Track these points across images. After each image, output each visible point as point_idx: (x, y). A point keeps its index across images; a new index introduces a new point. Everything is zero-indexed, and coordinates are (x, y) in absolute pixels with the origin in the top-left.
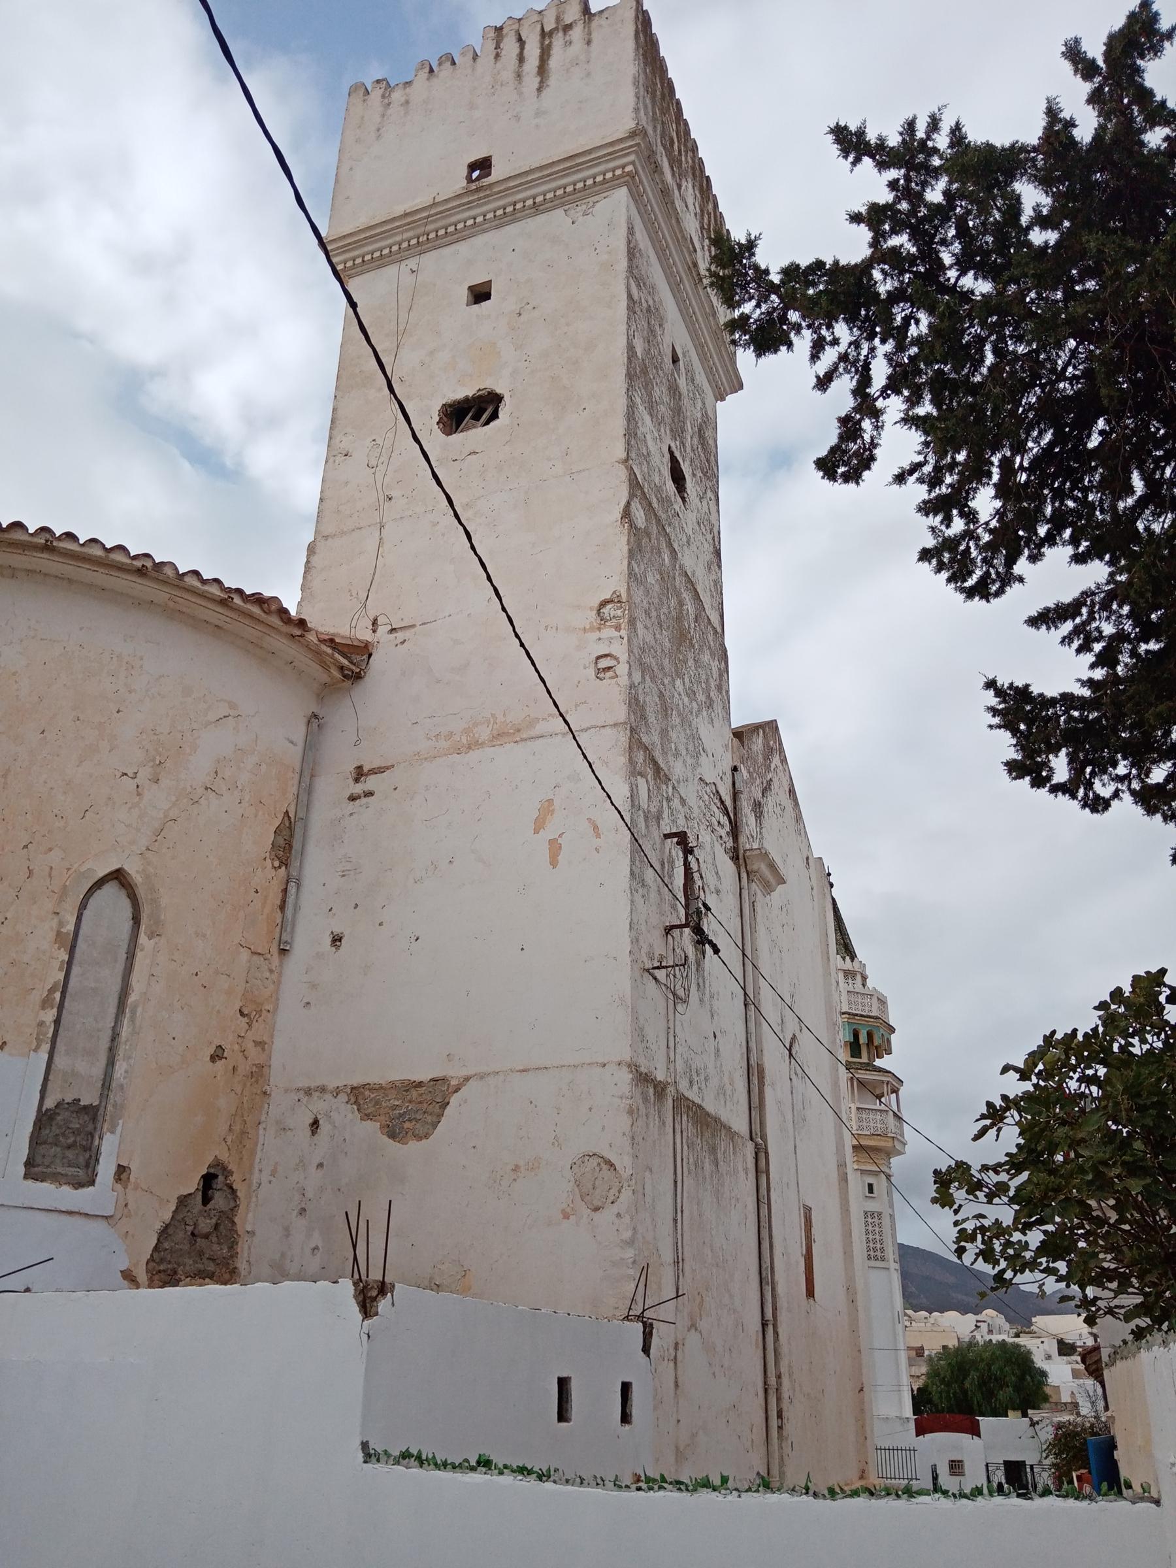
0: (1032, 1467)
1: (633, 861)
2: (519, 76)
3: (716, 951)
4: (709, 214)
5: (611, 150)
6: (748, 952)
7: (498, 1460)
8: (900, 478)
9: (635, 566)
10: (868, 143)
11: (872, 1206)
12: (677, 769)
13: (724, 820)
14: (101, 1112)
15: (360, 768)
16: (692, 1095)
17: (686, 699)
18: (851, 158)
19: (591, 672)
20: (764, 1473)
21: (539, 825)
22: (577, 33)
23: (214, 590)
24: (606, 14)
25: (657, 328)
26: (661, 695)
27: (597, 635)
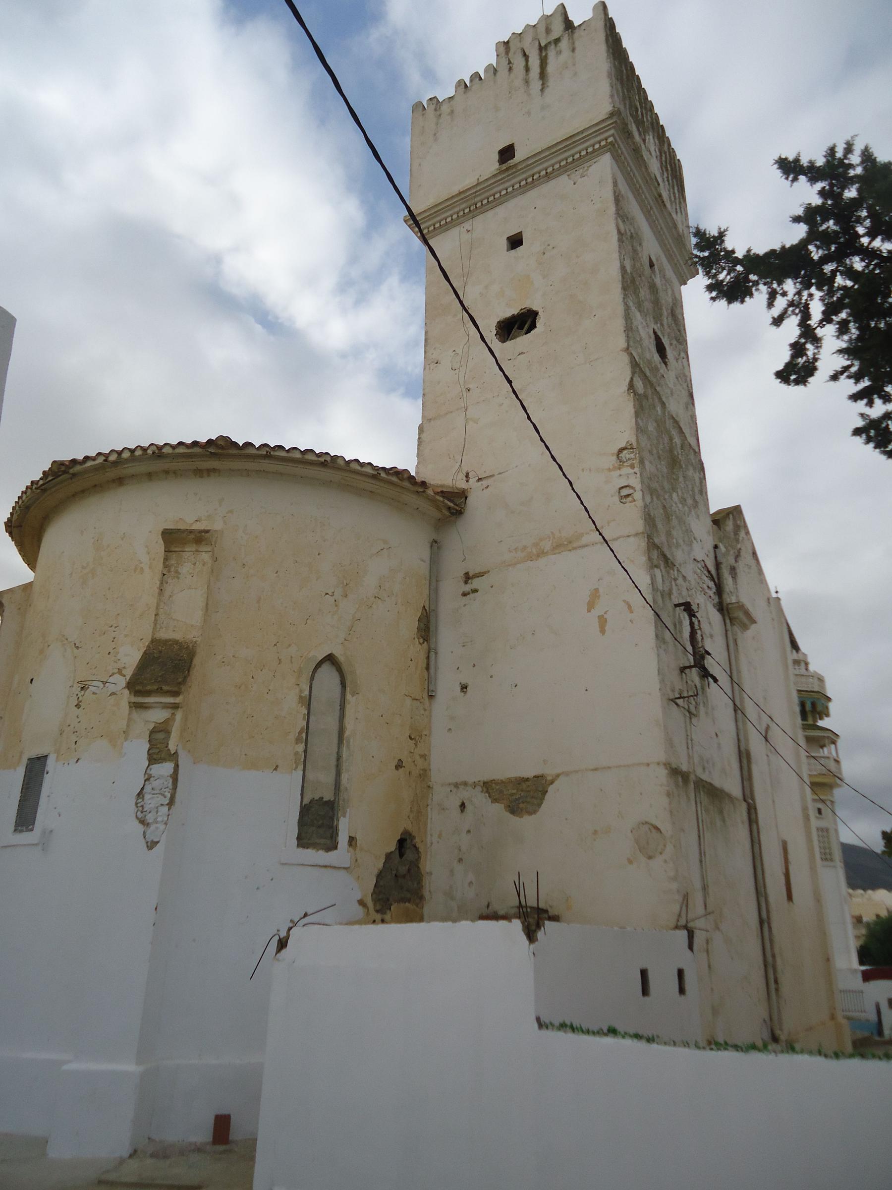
1: (656, 627)
2: (527, 82)
3: (716, 680)
4: (665, 153)
5: (597, 128)
6: (735, 679)
7: (621, 1028)
8: (835, 377)
9: (640, 421)
10: (802, 166)
11: (822, 824)
12: (678, 556)
13: (711, 584)
14: (336, 804)
15: (467, 574)
16: (705, 777)
17: (680, 506)
18: (791, 177)
19: (616, 499)
20: (767, 1019)
21: (591, 606)
22: (564, 44)
23: (369, 470)
24: (583, 27)
25: (639, 248)
26: (664, 507)
27: (618, 472)
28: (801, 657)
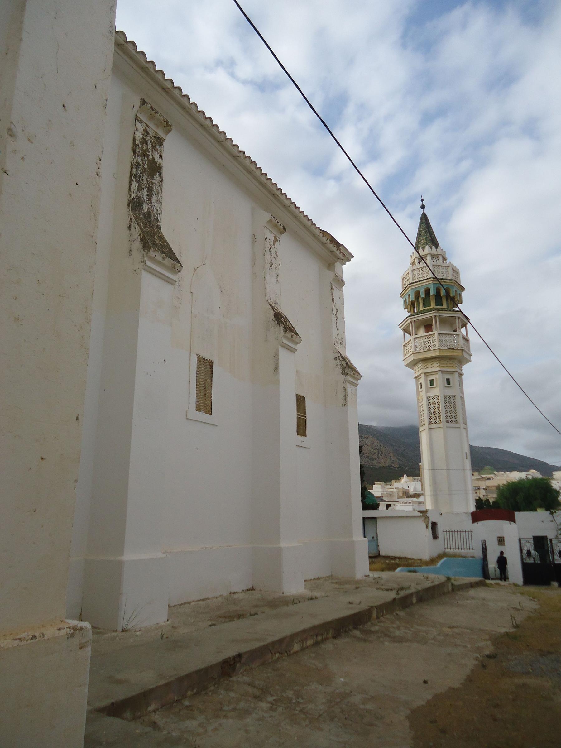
0: (551, 540)
11: (449, 392)
28: (439, 251)
